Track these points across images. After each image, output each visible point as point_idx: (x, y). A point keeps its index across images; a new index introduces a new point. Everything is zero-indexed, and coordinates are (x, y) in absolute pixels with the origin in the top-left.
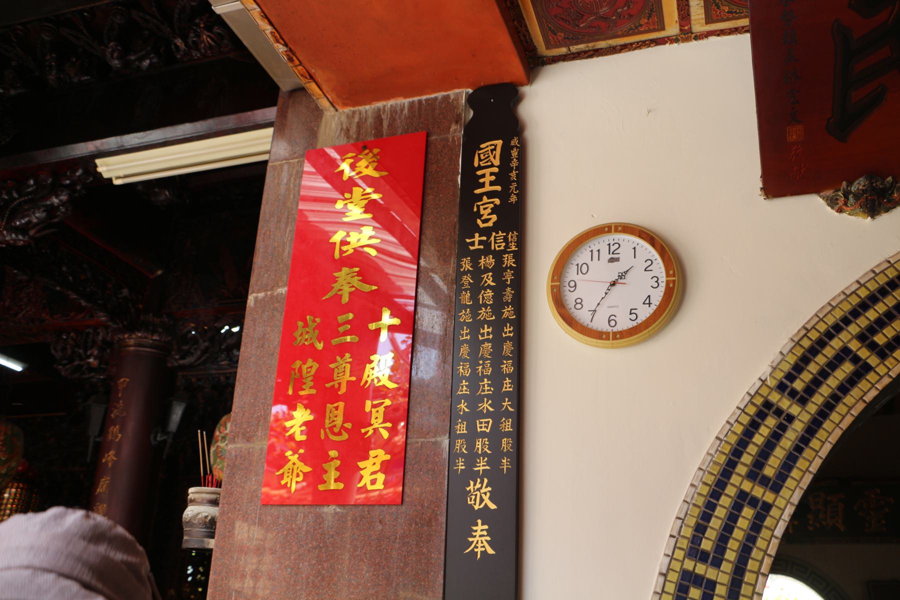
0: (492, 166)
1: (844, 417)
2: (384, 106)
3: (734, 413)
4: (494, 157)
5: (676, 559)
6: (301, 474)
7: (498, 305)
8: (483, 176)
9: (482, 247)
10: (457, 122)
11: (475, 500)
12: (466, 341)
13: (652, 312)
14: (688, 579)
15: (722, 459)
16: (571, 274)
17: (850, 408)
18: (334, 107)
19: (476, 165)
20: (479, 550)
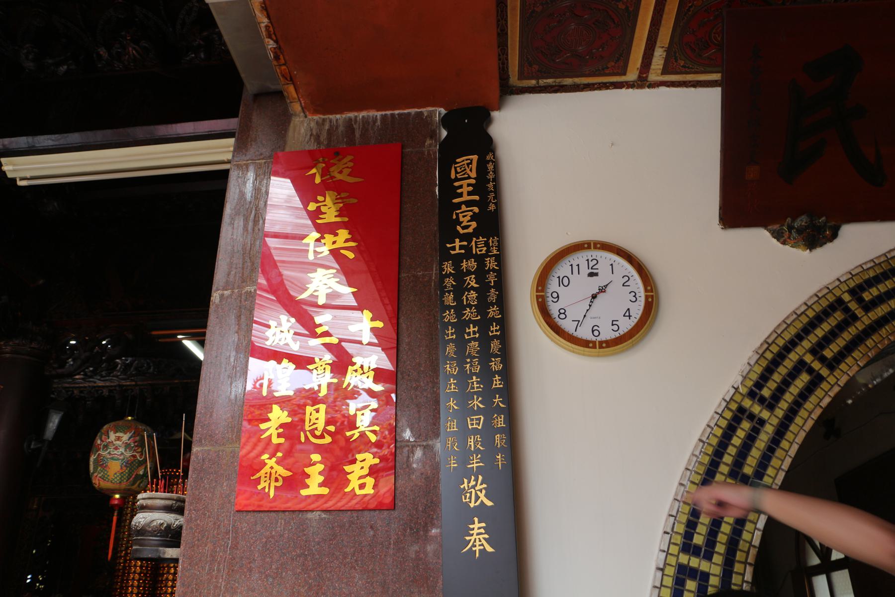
0: (469, 178)
1: (806, 421)
2: (356, 117)
3: (712, 418)
4: (471, 170)
5: (671, 554)
6: (280, 478)
7: (483, 306)
8: (461, 187)
9: (463, 251)
10: (431, 138)
11: (470, 498)
12: (452, 340)
13: (633, 324)
14: (684, 573)
15: (706, 460)
16: (553, 285)
17: (810, 413)
18: (304, 112)
19: (453, 176)
20: (477, 548)
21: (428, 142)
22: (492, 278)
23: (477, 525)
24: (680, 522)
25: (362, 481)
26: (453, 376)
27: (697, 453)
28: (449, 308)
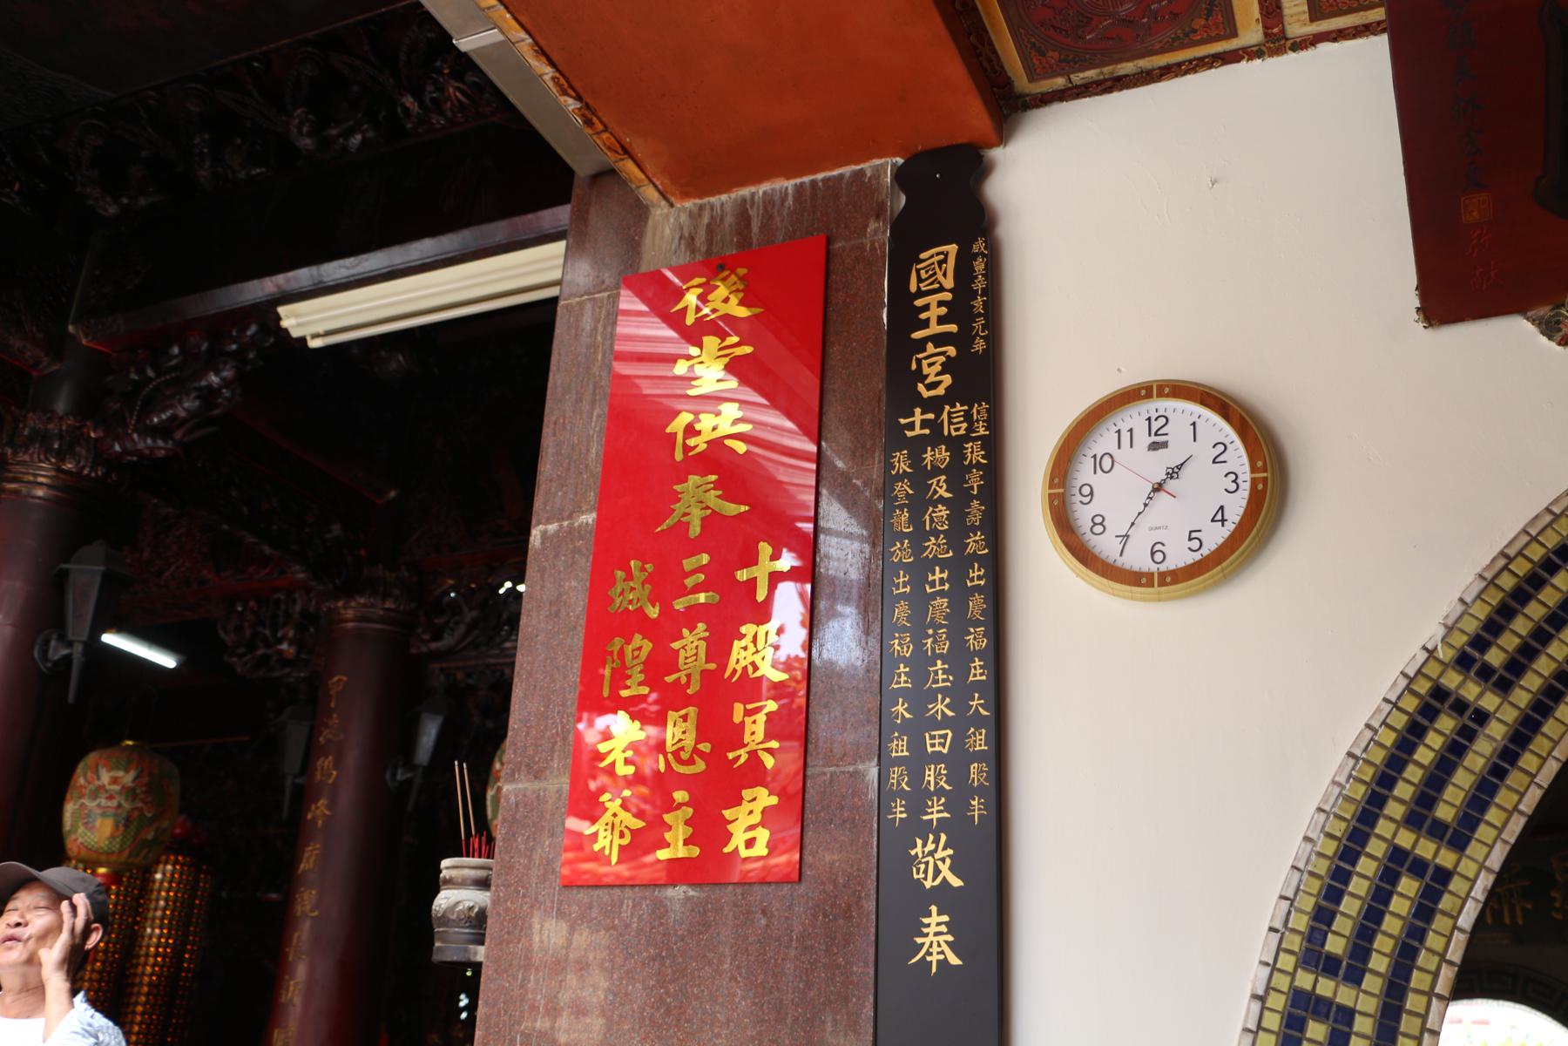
0: (941, 289)
2: (753, 194)
3: (1378, 710)
4: (945, 275)
5: (1281, 971)
6: (627, 833)
8: (926, 308)
9: (927, 431)
10: (878, 217)
11: (926, 872)
14: (1303, 1006)
15: (1360, 792)
16: (1084, 473)
19: (913, 288)
20: (934, 959)
21: (872, 225)
24: (1299, 911)
25: (750, 835)
26: (904, 660)
27: (1342, 779)
28: (901, 536)
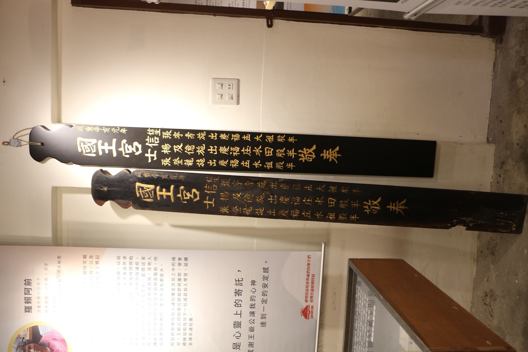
0: (96, 144)
8: (103, 151)
9: (155, 152)
19: (94, 155)
22: (177, 135)
23: (391, 207)
